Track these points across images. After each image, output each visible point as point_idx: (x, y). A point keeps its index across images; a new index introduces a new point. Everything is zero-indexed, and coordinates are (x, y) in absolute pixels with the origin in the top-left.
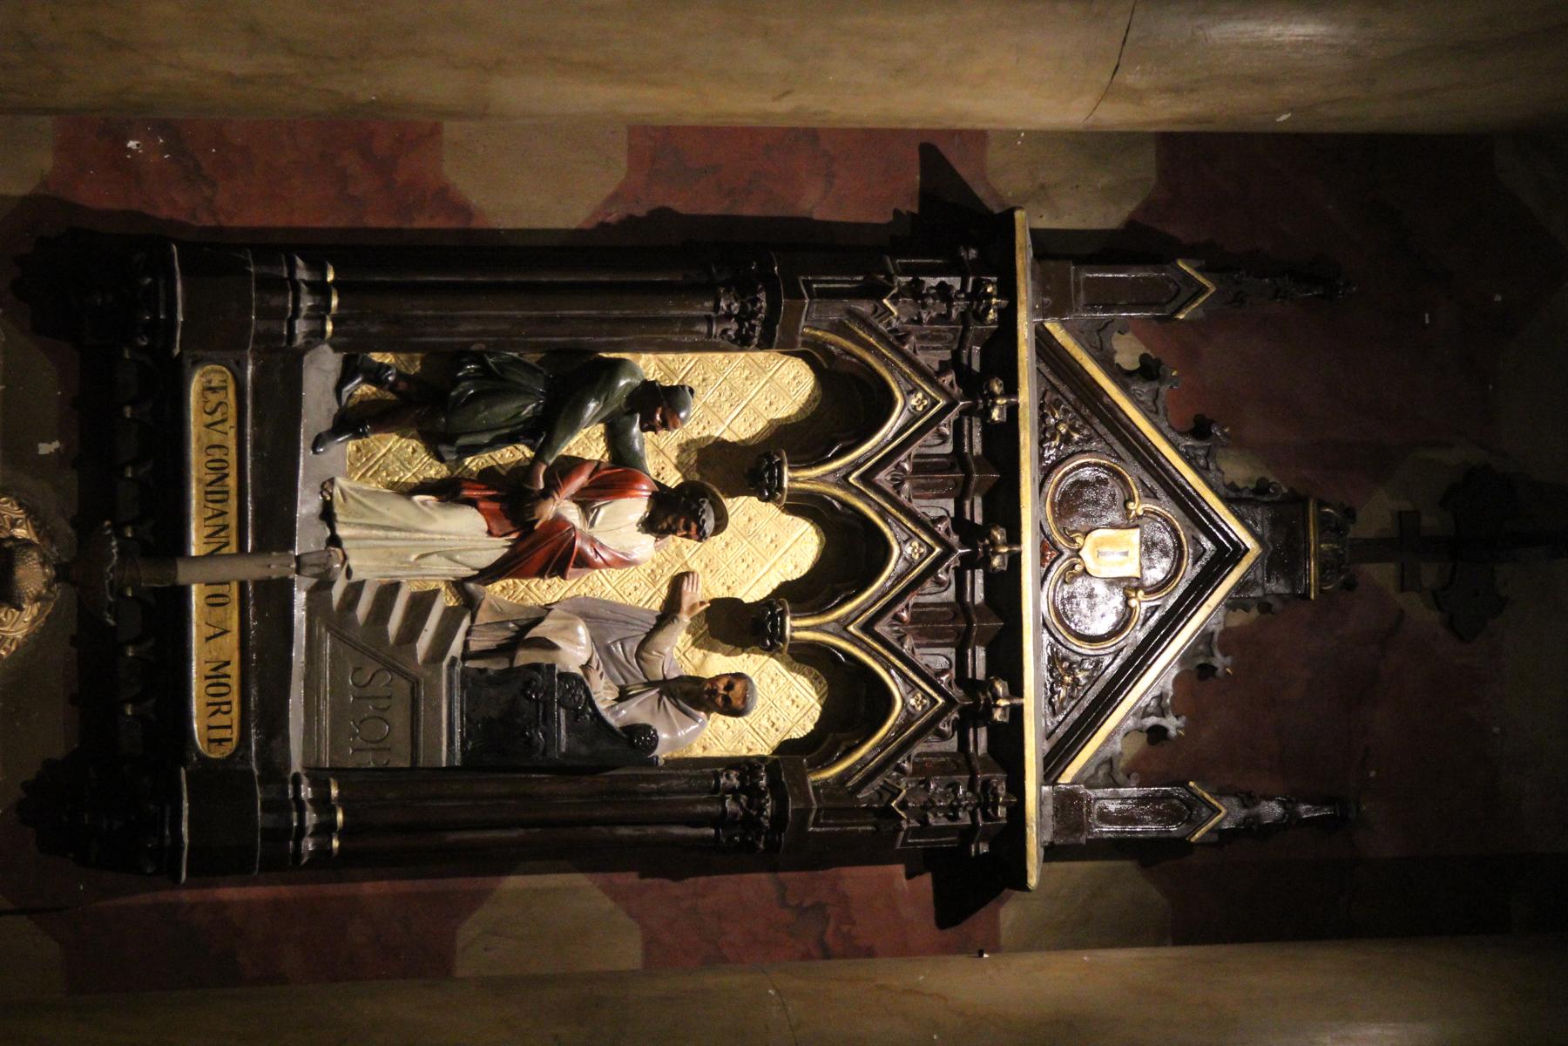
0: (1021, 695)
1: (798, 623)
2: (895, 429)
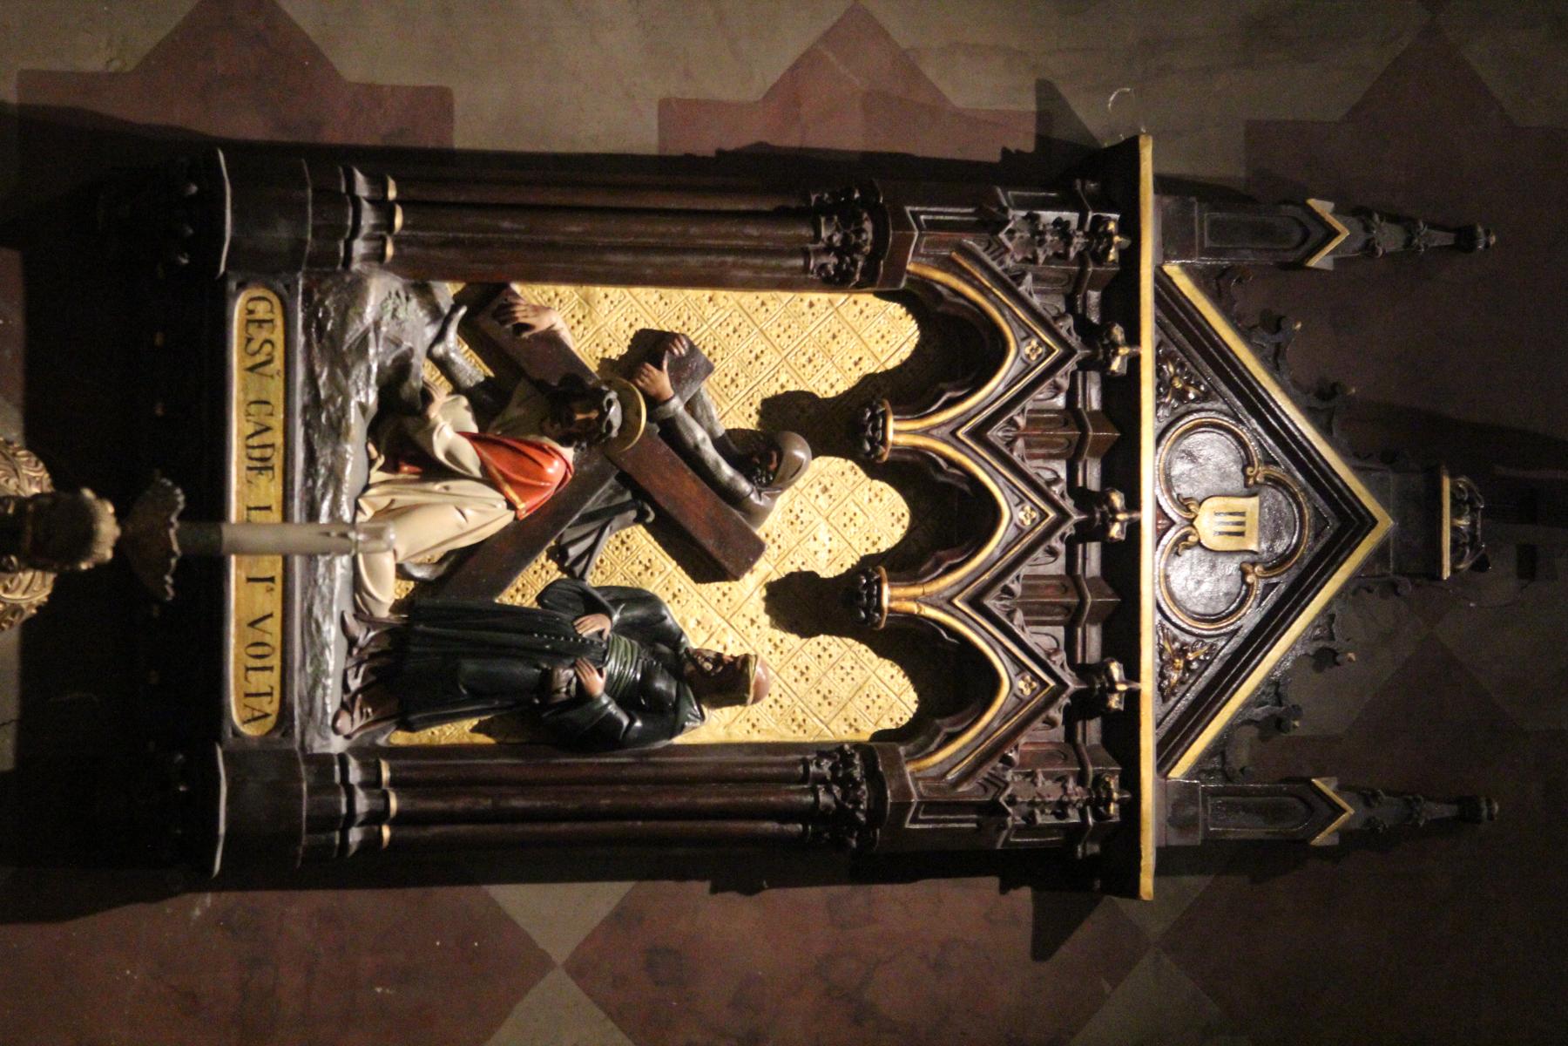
0: (1137, 679)
1: (900, 592)
2: (1010, 377)
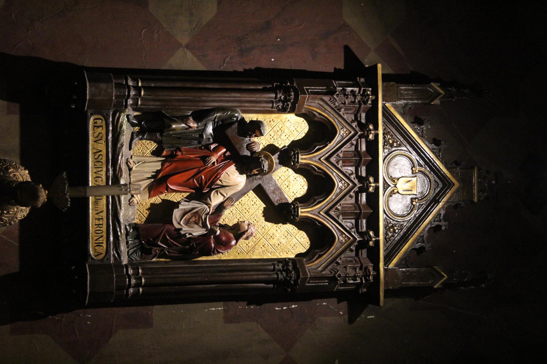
0: (379, 237)
1: (304, 157)
